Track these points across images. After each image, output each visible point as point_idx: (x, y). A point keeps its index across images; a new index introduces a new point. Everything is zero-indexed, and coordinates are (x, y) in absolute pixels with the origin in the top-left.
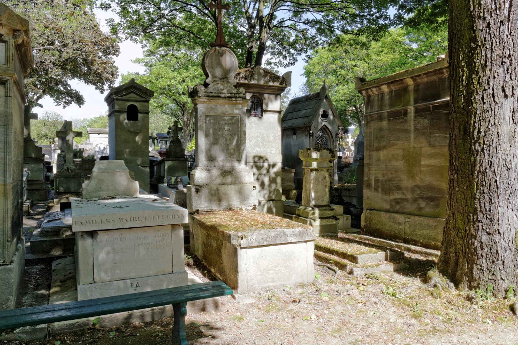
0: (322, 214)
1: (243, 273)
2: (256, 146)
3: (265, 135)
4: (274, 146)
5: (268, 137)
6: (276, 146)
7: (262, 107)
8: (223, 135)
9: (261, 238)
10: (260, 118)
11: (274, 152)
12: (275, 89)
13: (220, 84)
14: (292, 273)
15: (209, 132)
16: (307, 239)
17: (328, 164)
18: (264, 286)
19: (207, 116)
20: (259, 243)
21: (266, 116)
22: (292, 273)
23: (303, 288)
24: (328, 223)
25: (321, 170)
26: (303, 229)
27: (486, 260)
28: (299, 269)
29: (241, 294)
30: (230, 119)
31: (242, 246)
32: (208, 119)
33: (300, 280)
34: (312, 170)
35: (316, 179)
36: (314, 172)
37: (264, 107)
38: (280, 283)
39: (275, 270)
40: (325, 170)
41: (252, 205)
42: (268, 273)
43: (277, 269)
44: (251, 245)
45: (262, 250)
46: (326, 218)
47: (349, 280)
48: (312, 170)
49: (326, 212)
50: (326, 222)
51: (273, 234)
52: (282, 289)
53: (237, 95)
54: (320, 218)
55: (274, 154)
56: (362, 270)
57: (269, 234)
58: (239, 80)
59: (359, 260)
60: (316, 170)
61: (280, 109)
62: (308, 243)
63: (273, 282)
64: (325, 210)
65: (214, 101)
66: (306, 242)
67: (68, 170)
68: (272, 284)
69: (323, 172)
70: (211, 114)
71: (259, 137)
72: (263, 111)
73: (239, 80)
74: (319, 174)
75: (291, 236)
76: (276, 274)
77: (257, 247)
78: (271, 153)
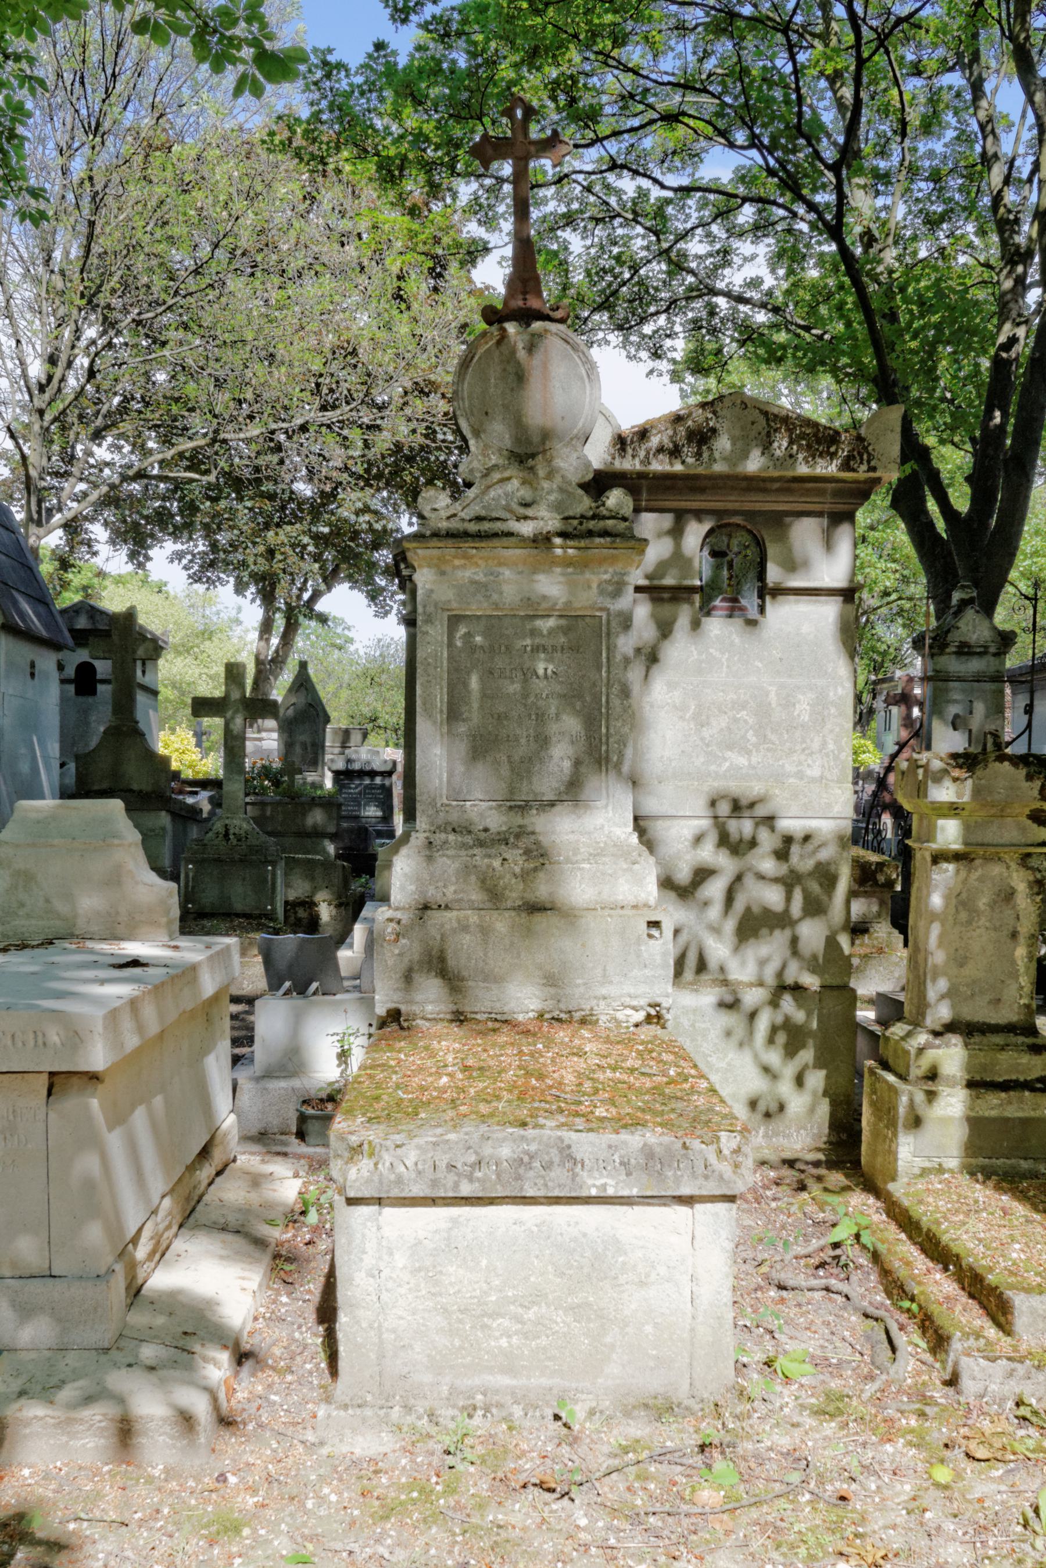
0: (984, 1068)
1: (361, 1313)
2: (730, 747)
3: (773, 698)
4: (816, 745)
5: (788, 704)
6: (824, 744)
7: (762, 576)
8: (525, 696)
9: (442, 1165)
10: (752, 623)
11: (815, 772)
12: (822, 492)
13: (515, 483)
14: (608, 1340)
15: (466, 685)
16: (686, 1191)
17: (1023, 830)
18: (466, 1383)
19: (454, 621)
20: (435, 1183)
21: (782, 615)
22: (608, 1340)
23: (659, 1419)
24: (1013, 1111)
25: (987, 859)
26: (667, 1139)
27: (526, 518)
28: (649, 1329)
29: (346, 1407)
30: (559, 628)
31: (352, 1194)
32: (462, 630)
33: (653, 1383)
34: (938, 858)
35: (961, 902)
36: (951, 867)
37: (774, 574)
38: (545, 1382)
39: (518, 1319)
40: (1011, 858)
41: (643, 1002)
42: (485, 1327)
43: (531, 1315)
44: (395, 1192)
45: (455, 1221)
46: (1005, 1086)
47: (922, 1414)
48: (938, 858)
49: (1005, 1058)
50: (994, 1105)
51: (506, 1152)
52: (549, 1413)
53: (592, 524)
54: (971, 1085)
55: (813, 780)
56: (1011, 1374)
57: (487, 1151)
58: (646, 461)
59: (1021, 1321)
60: (957, 857)
61: (851, 581)
62: (698, 1207)
63: (509, 1370)
64: (1003, 1048)
65: (484, 553)
66: (688, 1201)
67: (226, 835)
68: (505, 1381)
69: (996, 870)
70: (475, 609)
71: (744, 706)
72: (767, 592)
73: (646, 461)
74: (975, 875)
75: (602, 1165)
76: (526, 1335)
77: (432, 1201)
78: (800, 775)
